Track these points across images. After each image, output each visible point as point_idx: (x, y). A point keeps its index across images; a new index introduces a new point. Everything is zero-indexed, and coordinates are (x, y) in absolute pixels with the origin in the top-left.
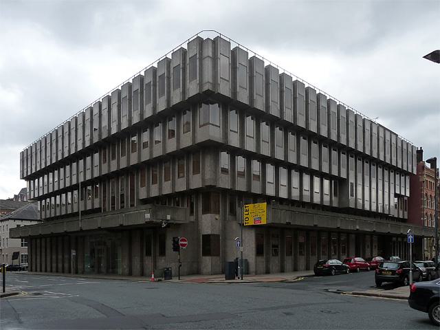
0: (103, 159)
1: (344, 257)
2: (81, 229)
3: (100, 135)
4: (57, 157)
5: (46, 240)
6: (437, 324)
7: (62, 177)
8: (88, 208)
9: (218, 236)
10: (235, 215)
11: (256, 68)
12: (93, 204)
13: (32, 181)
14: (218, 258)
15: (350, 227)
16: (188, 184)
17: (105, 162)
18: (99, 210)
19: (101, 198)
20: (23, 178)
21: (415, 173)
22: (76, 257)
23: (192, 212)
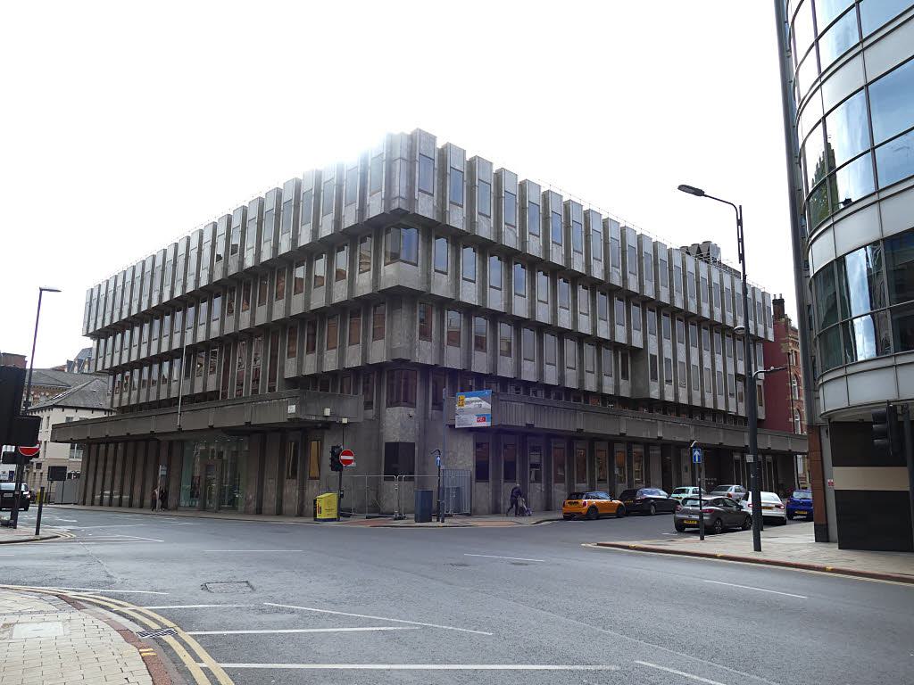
0: (228, 309)
1: (621, 488)
2: (180, 429)
3: (225, 269)
4: (150, 301)
5: (116, 448)
7: (146, 338)
8: (196, 392)
9: (413, 445)
10: (441, 409)
11: (479, 174)
12: (205, 385)
13: (103, 341)
15: (646, 434)
16: (365, 355)
17: (231, 312)
19: (219, 375)
20: (87, 335)
21: (771, 338)
22: (167, 477)
23: (368, 405)
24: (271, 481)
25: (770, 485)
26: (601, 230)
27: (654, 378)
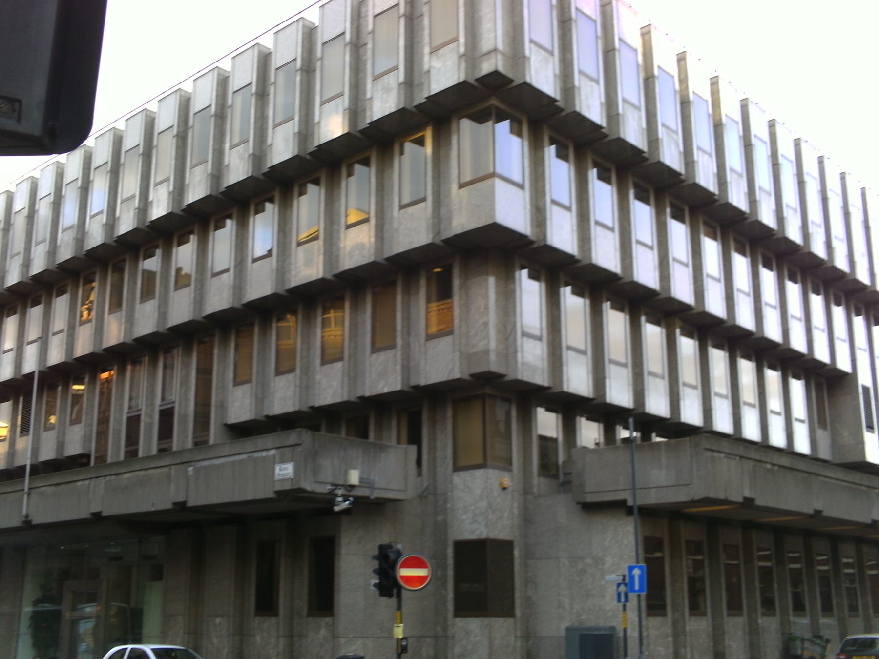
6: (399, 656)
9: (507, 546)
14: (510, 620)
16: (407, 370)
18: (79, 462)
24: (218, 620)
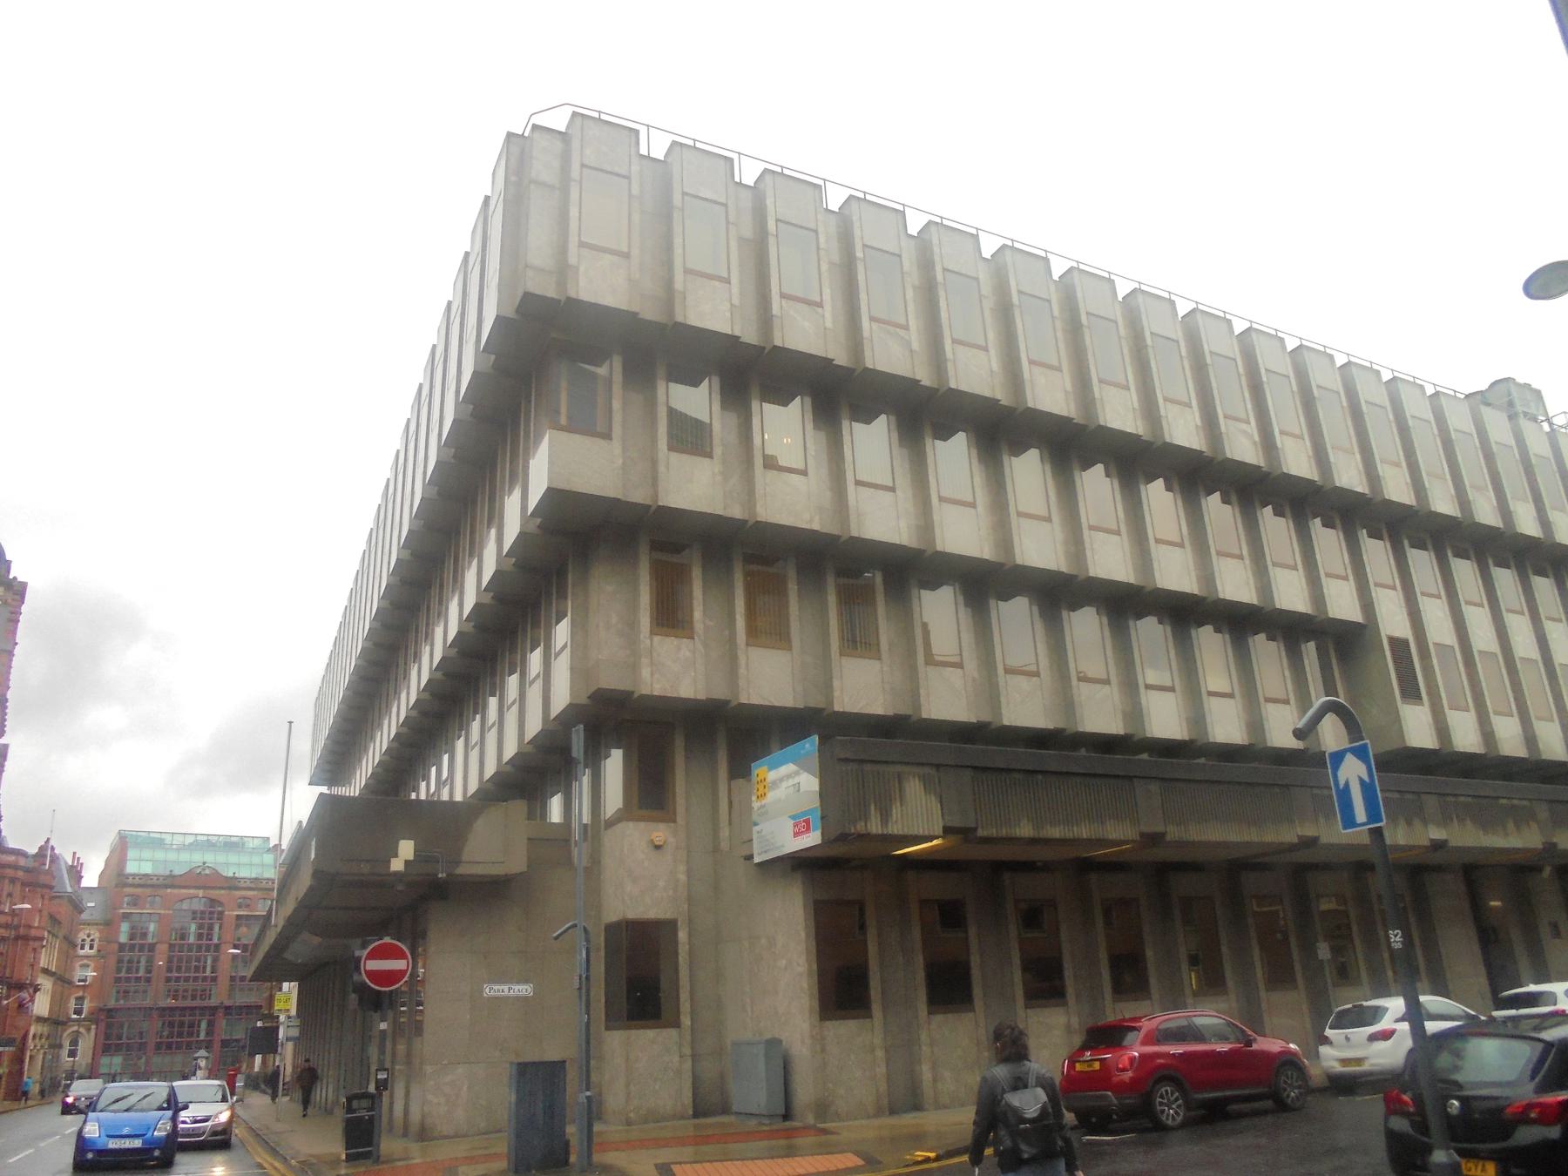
25: (419, 856)
26: (1512, 442)
27: (1411, 693)
